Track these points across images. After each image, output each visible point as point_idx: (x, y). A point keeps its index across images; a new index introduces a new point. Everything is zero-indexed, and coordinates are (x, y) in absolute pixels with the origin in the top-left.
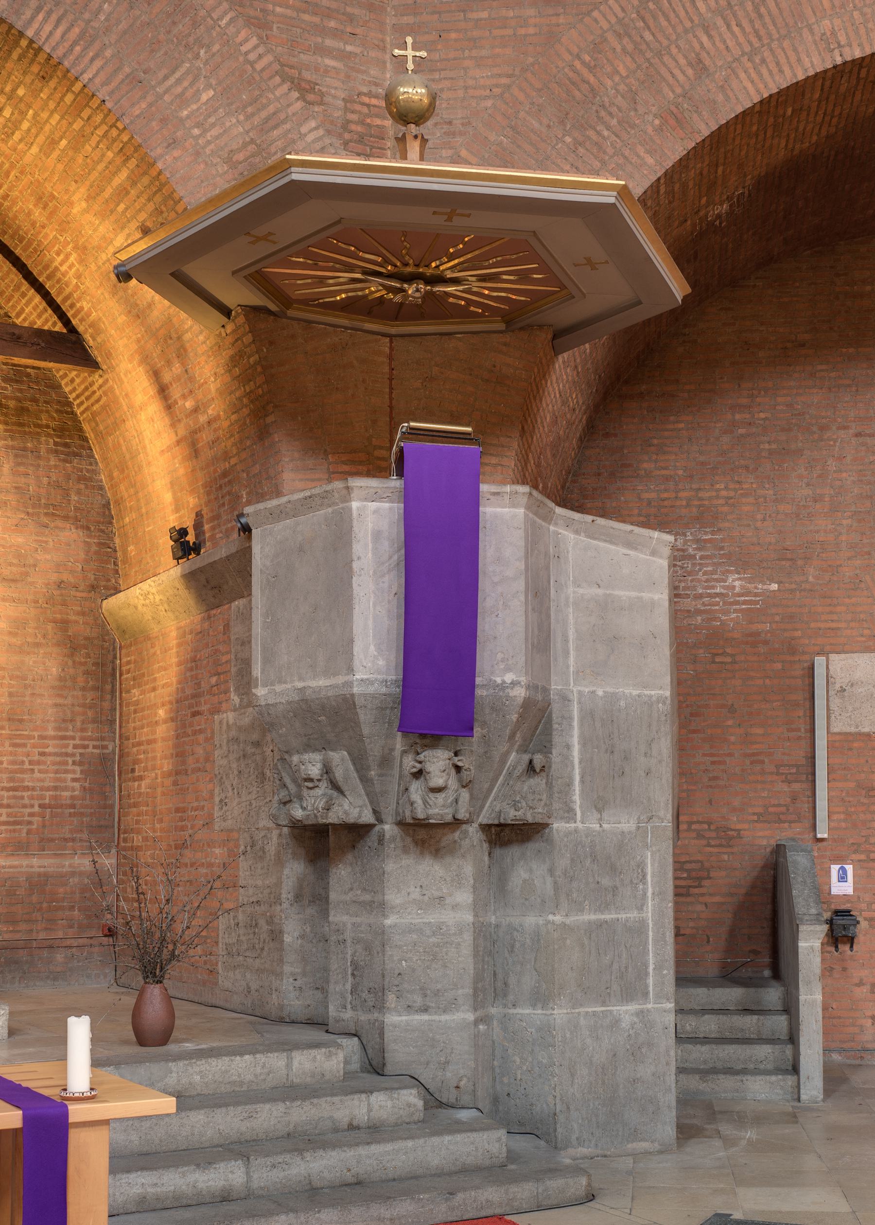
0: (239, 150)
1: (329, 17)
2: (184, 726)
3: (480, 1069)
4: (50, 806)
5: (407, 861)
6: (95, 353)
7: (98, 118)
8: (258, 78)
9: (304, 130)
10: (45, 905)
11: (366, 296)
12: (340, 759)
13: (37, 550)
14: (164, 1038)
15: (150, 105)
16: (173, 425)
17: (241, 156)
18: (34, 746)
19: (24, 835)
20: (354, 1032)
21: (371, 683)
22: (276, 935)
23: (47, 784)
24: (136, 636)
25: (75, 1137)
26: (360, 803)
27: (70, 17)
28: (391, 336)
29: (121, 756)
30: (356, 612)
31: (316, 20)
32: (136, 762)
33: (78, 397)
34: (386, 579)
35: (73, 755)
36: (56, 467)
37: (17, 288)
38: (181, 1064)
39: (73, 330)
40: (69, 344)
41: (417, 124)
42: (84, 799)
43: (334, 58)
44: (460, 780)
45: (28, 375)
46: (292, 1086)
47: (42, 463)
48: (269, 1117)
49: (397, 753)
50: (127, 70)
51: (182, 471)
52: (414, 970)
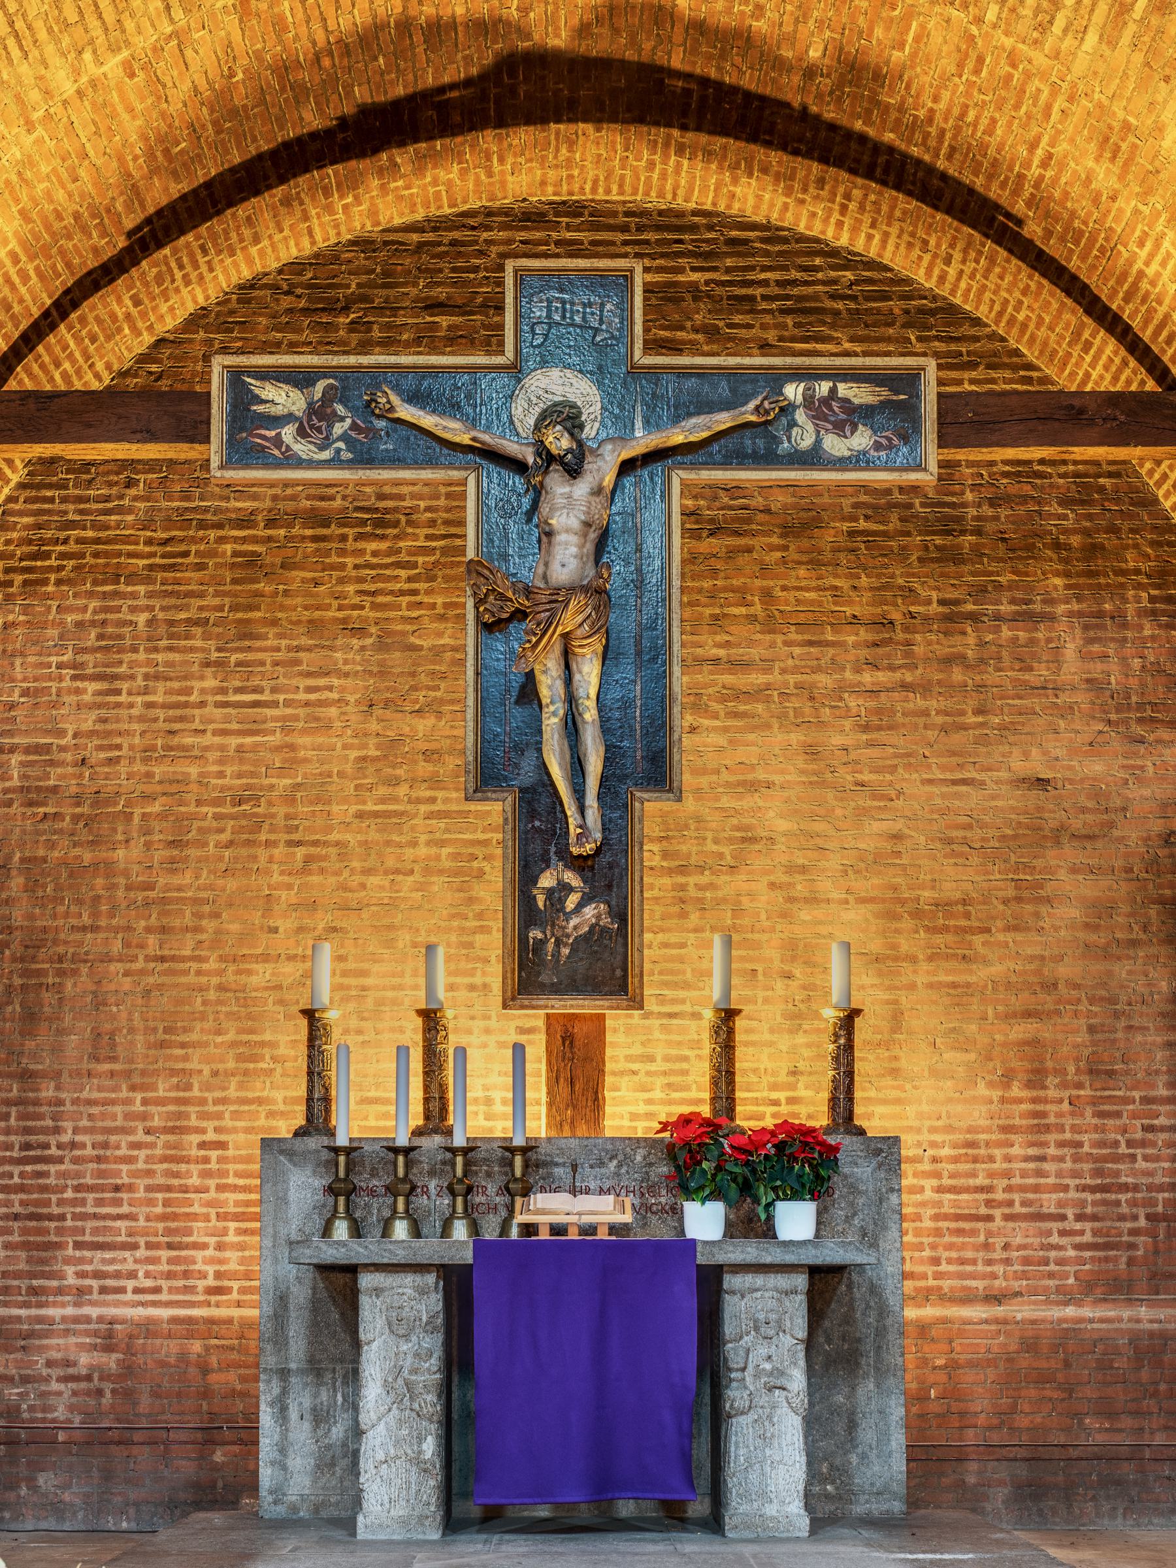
4: (1165, 1218)
10: (1163, 1387)
13: (1126, 782)
18: (1134, 1116)
19: (1123, 1266)
23: (1159, 1179)
36: (1153, 638)
45: (1102, 489)
47: (1129, 634)
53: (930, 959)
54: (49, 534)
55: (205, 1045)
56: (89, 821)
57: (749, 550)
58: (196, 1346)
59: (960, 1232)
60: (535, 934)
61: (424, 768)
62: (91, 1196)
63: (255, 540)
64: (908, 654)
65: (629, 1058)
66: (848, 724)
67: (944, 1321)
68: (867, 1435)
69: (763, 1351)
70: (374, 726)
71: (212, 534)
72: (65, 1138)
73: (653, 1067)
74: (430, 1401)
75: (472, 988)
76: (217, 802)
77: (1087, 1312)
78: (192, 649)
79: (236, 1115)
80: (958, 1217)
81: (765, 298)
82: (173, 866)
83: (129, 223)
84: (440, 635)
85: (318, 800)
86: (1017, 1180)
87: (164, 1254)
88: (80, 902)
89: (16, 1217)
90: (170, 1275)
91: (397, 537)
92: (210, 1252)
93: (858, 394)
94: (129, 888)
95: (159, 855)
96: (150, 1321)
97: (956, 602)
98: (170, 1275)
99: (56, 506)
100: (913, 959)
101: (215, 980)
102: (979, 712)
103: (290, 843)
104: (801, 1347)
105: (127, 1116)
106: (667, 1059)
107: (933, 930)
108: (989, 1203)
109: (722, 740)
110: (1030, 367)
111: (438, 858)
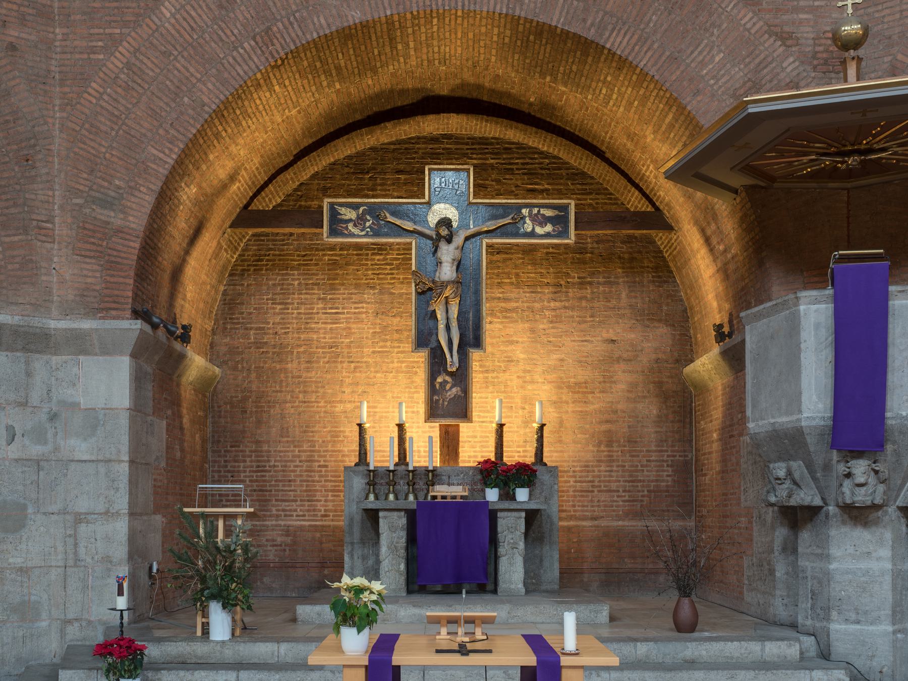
0: (741, 88)
3: (898, 662)
4: (654, 491)
5: (845, 529)
6: (670, 221)
7: (652, 86)
8: (752, 38)
9: (784, 65)
11: (823, 168)
12: (798, 467)
14: (692, 628)
15: (683, 72)
16: (714, 261)
18: (644, 456)
20: (812, 632)
21: (814, 419)
22: (772, 572)
23: (652, 478)
24: (701, 389)
25: (564, 673)
26: (812, 493)
27: (632, 29)
28: (848, 190)
29: (696, 461)
30: (803, 376)
32: (703, 465)
34: (824, 353)
35: (667, 461)
36: (653, 290)
37: (625, 187)
38: (694, 644)
39: (657, 209)
40: (657, 218)
41: (855, 49)
42: (674, 487)
43: (807, 13)
44: (878, 479)
46: (765, 662)
49: (834, 462)
50: (668, 53)
51: (721, 288)
52: (850, 597)
53: (573, 402)
54: (263, 253)
55: (320, 432)
56: (279, 354)
57: (511, 259)
58: (318, 535)
59: (582, 496)
60: (436, 397)
61: (396, 336)
62: (281, 484)
63: (336, 255)
64: (567, 296)
65: (468, 437)
66: (545, 321)
67: (577, 526)
68: (546, 564)
69: (510, 536)
70: (378, 321)
71: (321, 253)
72: (272, 464)
73: (476, 440)
74: (402, 552)
75: (413, 412)
76: (323, 347)
77: (626, 523)
78: (314, 294)
79: (331, 456)
80: (582, 491)
81: (517, 169)
82: (308, 370)
83: (295, 153)
84: (402, 289)
85: (359, 347)
86: (603, 479)
87: (307, 503)
88: (275, 382)
89: (255, 491)
90: (308, 511)
91: (386, 254)
92: (322, 503)
93: (548, 213)
94: (293, 377)
95: (303, 366)
96: (302, 526)
97: (584, 278)
98: (308, 511)
99: (265, 242)
100: (567, 403)
101: (323, 409)
102: (592, 316)
103: (349, 362)
104: (523, 536)
105: (293, 456)
106: (481, 437)
107: (574, 393)
108: (593, 486)
109: (501, 327)
110: (611, 194)
111: (401, 367)
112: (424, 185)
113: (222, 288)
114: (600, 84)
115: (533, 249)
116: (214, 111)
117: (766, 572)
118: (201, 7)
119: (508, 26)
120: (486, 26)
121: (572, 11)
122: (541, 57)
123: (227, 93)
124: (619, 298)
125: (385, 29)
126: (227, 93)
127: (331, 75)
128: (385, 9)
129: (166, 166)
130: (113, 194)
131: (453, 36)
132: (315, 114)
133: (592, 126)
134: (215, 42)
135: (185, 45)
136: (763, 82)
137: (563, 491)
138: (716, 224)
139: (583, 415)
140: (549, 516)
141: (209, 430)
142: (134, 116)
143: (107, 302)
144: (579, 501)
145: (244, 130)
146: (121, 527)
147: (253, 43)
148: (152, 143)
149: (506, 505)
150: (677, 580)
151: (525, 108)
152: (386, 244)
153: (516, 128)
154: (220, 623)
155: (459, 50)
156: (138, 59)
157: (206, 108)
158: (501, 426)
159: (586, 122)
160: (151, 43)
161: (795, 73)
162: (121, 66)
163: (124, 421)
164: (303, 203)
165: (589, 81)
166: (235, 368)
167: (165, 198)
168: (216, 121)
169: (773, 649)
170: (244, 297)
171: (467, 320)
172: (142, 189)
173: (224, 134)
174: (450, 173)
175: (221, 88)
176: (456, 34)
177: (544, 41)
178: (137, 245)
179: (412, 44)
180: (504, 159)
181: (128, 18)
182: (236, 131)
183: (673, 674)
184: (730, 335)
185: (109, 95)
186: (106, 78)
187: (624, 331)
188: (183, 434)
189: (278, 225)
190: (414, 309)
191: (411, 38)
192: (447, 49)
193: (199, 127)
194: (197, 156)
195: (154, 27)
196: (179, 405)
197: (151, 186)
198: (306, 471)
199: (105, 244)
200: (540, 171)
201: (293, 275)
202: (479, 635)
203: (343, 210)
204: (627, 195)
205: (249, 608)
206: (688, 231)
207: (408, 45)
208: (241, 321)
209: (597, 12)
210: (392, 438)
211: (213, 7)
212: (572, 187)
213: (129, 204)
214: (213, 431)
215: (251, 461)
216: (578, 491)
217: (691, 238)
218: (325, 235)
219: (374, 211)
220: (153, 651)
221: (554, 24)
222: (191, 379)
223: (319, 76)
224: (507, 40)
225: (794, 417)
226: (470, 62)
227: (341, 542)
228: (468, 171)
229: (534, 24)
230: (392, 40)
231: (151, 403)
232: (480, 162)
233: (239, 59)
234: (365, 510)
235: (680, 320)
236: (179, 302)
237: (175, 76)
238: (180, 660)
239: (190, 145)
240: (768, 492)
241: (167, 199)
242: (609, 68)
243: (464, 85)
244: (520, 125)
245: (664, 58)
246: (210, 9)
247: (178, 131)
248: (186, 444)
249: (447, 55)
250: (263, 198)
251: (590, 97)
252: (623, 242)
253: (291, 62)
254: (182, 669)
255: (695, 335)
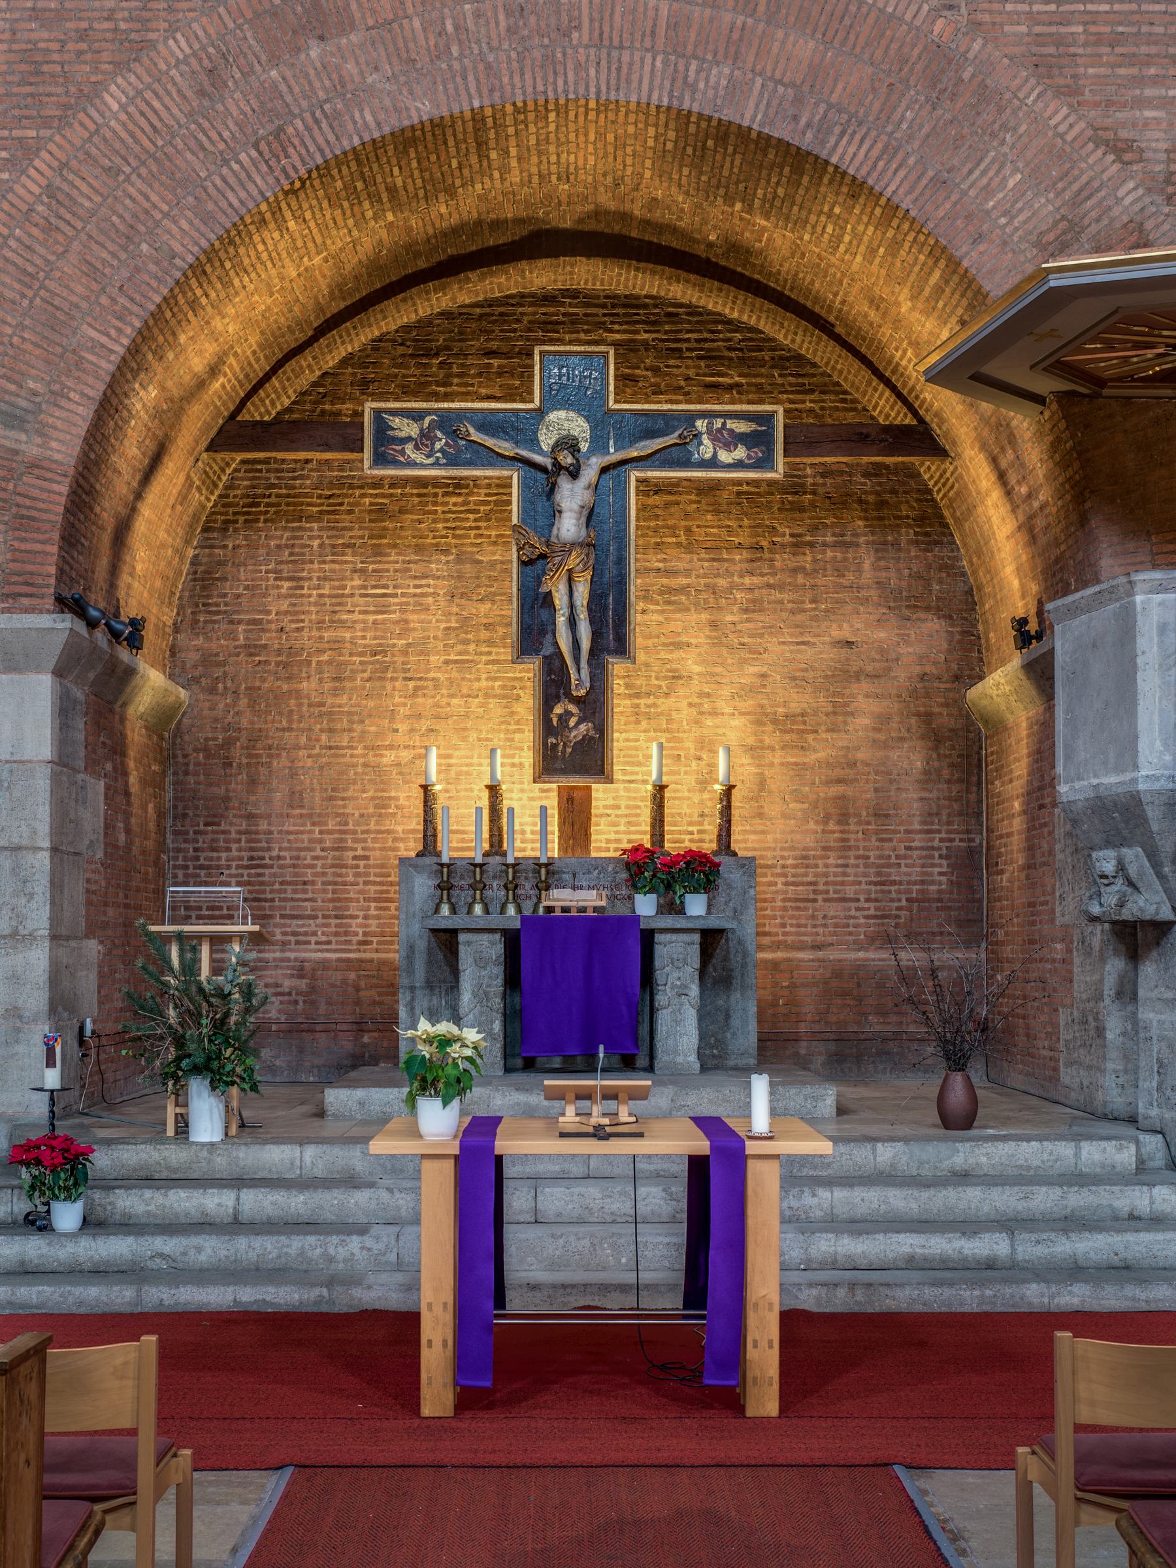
0: (1049, 230)
1: (1148, 64)
2: (1033, 819)
4: (917, 900)
6: (942, 441)
7: (906, 226)
8: (1068, 150)
9: (1120, 193)
12: (1134, 856)
16: (1013, 511)
17: (1051, 237)
18: (900, 841)
21: (1157, 779)
22: (1100, 1031)
23: (914, 878)
24: (997, 726)
25: (751, 1164)
26: (1157, 899)
27: (873, 133)
29: (988, 849)
30: (1141, 708)
31: (1134, 71)
32: (999, 855)
33: (936, 483)
35: (939, 849)
36: (916, 557)
37: (869, 383)
38: (967, 1145)
39: (921, 421)
40: (921, 438)
42: (951, 893)
43: (1156, 108)
46: (1081, 1175)
48: (1044, 1199)
50: (931, 173)
51: (1024, 558)
53: (782, 748)
54: (260, 491)
56: (286, 665)
57: (678, 503)
58: (352, 975)
59: (798, 909)
61: (484, 635)
63: (383, 496)
64: (771, 567)
65: (605, 807)
66: (735, 608)
67: (788, 960)
68: (736, 1022)
69: (676, 975)
70: (455, 609)
71: (357, 492)
72: (275, 853)
73: (619, 812)
74: (497, 1002)
75: (513, 765)
78: (346, 562)
79: (375, 840)
80: (797, 900)
81: (688, 349)
82: (335, 692)
83: (315, 325)
84: (494, 554)
85: (421, 653)
86: (831, 879)
87: (333, 921)
88: (281, 714)
90: (336, 934)
93: (740, 427)
94: (310, 705)
95: (328, 685)
97: (800, 535)
98: (336, 934)
99: (264, 474)
100: (772, 749)
101: (361, 760)
102: (813, 601)
103: (405, 679)
105: (310, 841)
106: (628, 807)
107: (783, 731)
108: (815, 892)
109: (661, 618)
110: (845, 392)
111: (493, 688)
112: (532, 376)
113: (191, 552)
114: (823, 218)
115: (713, 487)
116: (191, 266)
117: (1092, 1033)
118: (169, 93)
119: (672, 125)
120: (636, 123)
121: (775, 103)
122: (726, 173)
123: (213, 237)
124: (859, 571)
125: (470, 129)
126: (213, 237)
127: (380, 201)
128: (470, 96)
129: (112, 358)
130: (24, 404)
131: (582, 138)
132: (351, 262)
133: (812, 282)
134: (193, 153)
135: (143, 157)
136: (1086, 222)
137: (765, 900)
138: (1015, 451)
139: (799, 769)
140: (740, 942)
141: (169, 795)
142: (58, 274)
143: (14, 583)
144: (792, 917)
145: (237, 293)
146: (37, 959)
147: (254, 153)
148: (89, 319)
149: (669, 921)
150: (943, 1042)
151: (700, 250)
152: (467, 478)
153: (687, 281)
154: (207, 1116)
155: (591, 160)
156: (66, 180)
157: (178, 261)
158: (660, 789)
159: (801, 275)
160: (87, 153)
161: (1139, 206)
162: (37, 191)
163: (42, 783)
164: (327, 407)
165: (804, 213)
166: (212, 690)
167: (109, 408)
168: (194, 283)
169: (1095, 1153)
170: (229, 568)
171: (605, 608)
172: (72, 395)
173: (204, 301)
174: (577, 360)
175: (203, 228)
176: (586, 135)
177: (730, 149)
178: (64, 489)
179: (513, 151)
180: (666, 332)
181: (51, 113)
182: (223, 295)
183: (932, 1191)
184: (1039, 636)
185: (18, 240)
186: (13, 211)
187: (867, 627)
188: (129, 803)
189: (282, 443)
190: (515, 590)
191: (512, 142)
192: (572, 158)
193: (165, 291)
194: (161, 339)
195: (92, 127)
196: (123, 754)
197: (87, 391)
198: (333, 866)
199: (11, 486)
200: (727, 353)
201: (311, 529)
202: (624, 1116)
203: (396, 422)
204: (872, 396)
205: (254, 1088)
206: (971, 459)
207: (507, 152)
208: (222, 608)
209: (816, 105)
210: (479, 810)
211: (189, 93)
212: (780, 381)
213: (51, 420)
214: (176, 798)
215: (240, 850)
216: (790, 900)
217: (975, 469)
218: (366, 464)
219: (449, 424)
220: (102, 1161)
221: (746, 123)
222: (141, 709)
223: (360, 203)
224: (670, 146)
225: (1127, 776)
226: (609, 179)
227: (392, 989)
228: (605, 355)
229: (714, 123)
230: (481, 145)
231: (82, 753)
232: (625, 336)
233: (232, 180)
234: (433, 931)
235: (962, 607)
236: (125, 578)
237: (126, 208)
238: (143, 1174)
239: (151, 322)
240: (1091, 898)
241: (112, 411)
242: (837, 194)
243: (598, 214)
244: (692, 277)
245: (924, 182)
246: (185, 97)
247: (132, 299)
248: (133, 820)
249: (572, 169)
250: (262, 401)
251: (807, 237)
252: (866, 475)
253: (316, 183)
254: (149, 1187)
255: (986, 634)
